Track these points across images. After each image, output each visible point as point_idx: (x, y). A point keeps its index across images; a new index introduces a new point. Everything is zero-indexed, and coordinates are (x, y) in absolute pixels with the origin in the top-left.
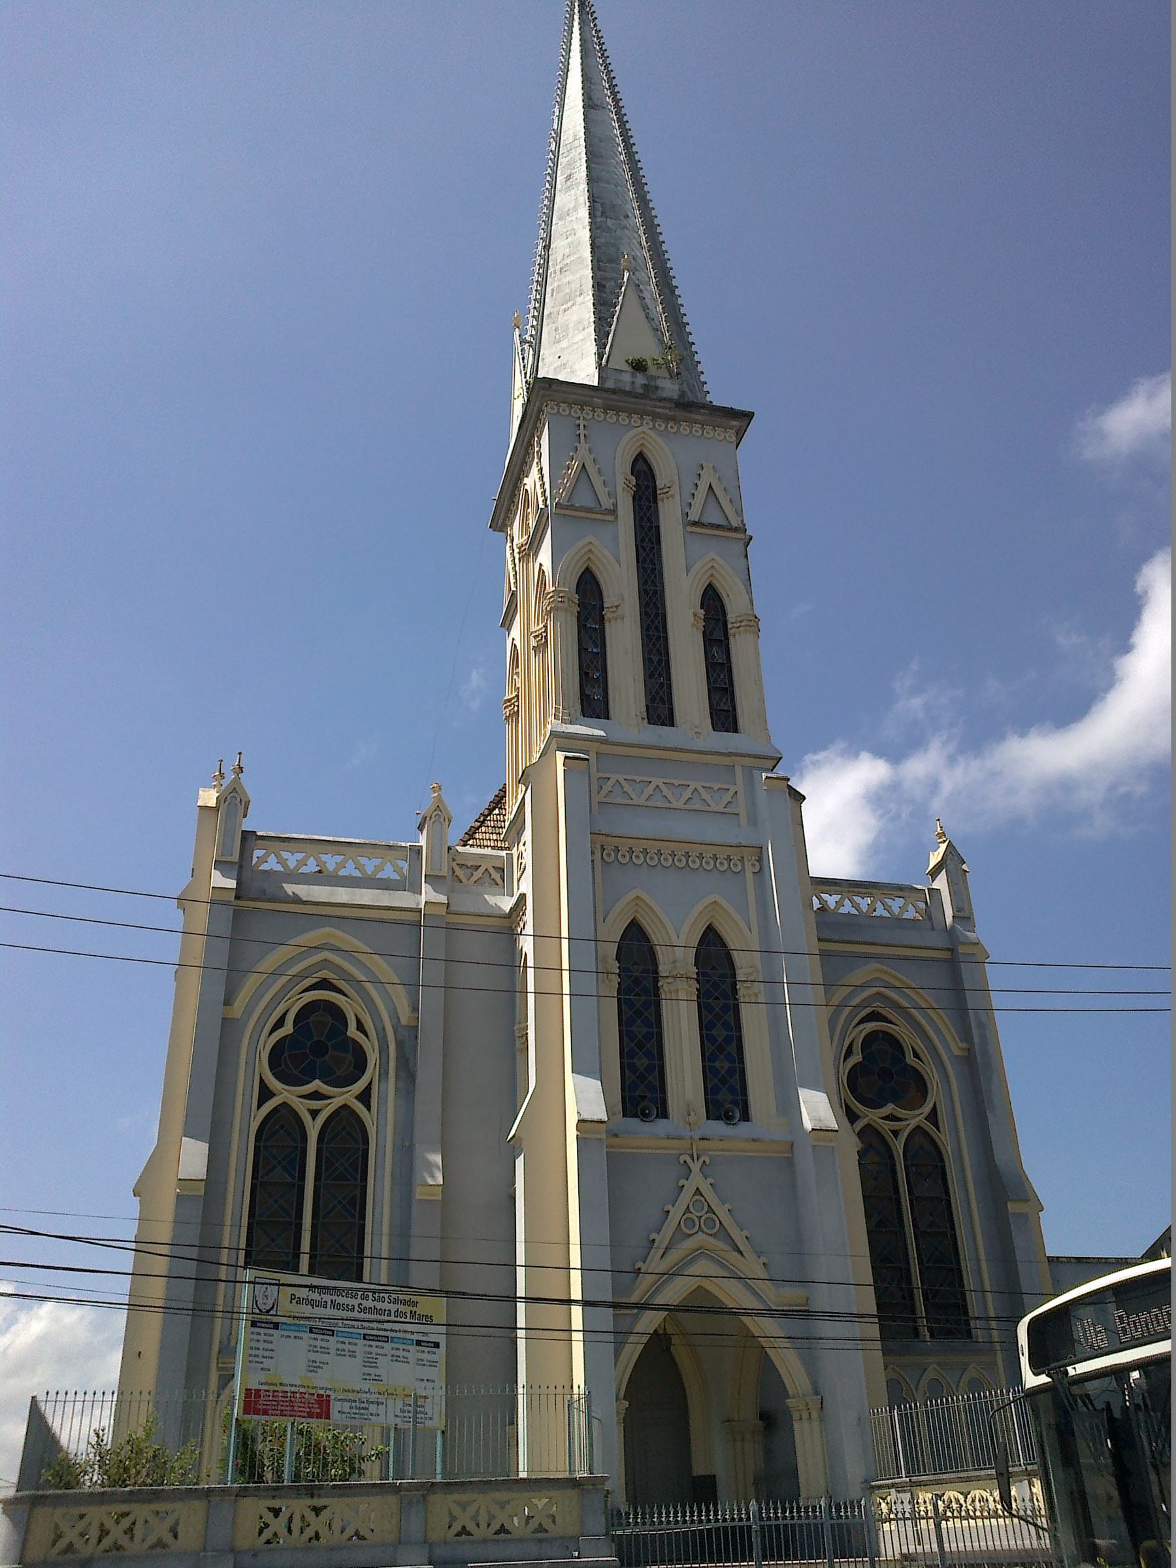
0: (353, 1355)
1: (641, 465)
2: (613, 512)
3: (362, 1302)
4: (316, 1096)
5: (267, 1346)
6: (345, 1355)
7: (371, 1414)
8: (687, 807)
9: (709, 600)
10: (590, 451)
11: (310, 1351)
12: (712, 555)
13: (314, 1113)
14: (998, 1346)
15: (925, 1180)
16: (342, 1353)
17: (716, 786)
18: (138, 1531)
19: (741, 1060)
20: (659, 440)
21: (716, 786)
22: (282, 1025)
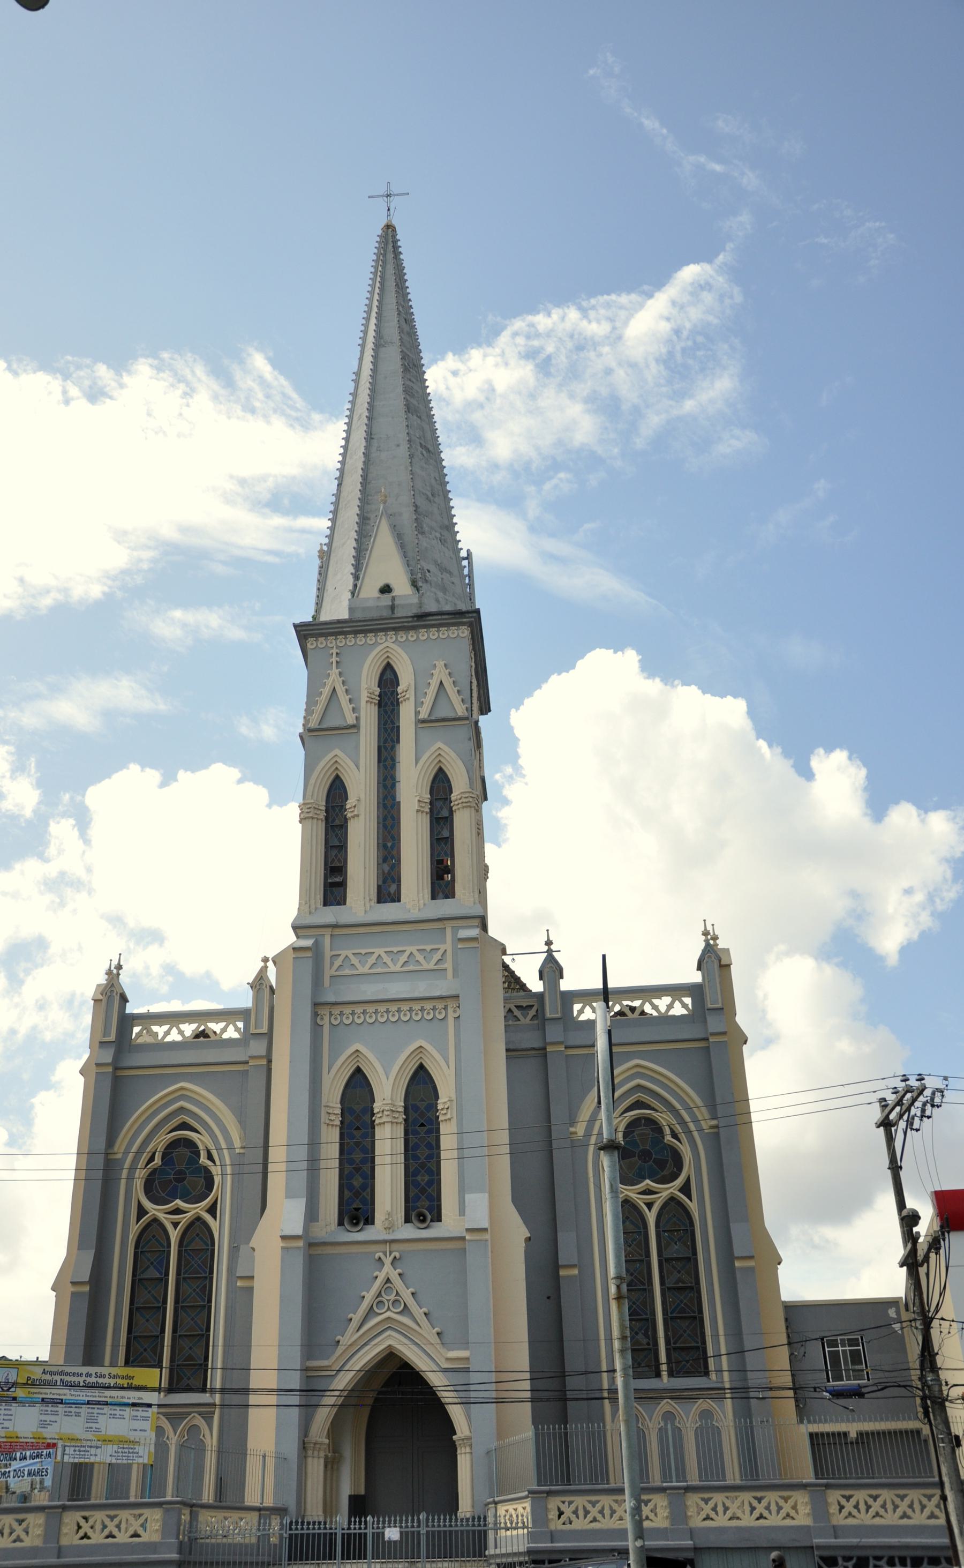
0: (78, 1415)
1: (388, 675)
2: (356, 726)
3: (86, 1379)
4: (178, 1211)
5: (7, 1412)
6: (72, 1416)
7: (91, 1455)
8: (405, 969)
9: (439, 782)
10: (340, 674)
11: (41, 1414)
12: (439, 744)
13: (175, 1225)
14: (606, 1395)
15: (676, 1243)
16: (69, 1414)
17: (428, 948)
18: (123, 1526)
19: (439, 1174)
20: (400, 650)
21: (428, 948)
22: (154, 1161)
